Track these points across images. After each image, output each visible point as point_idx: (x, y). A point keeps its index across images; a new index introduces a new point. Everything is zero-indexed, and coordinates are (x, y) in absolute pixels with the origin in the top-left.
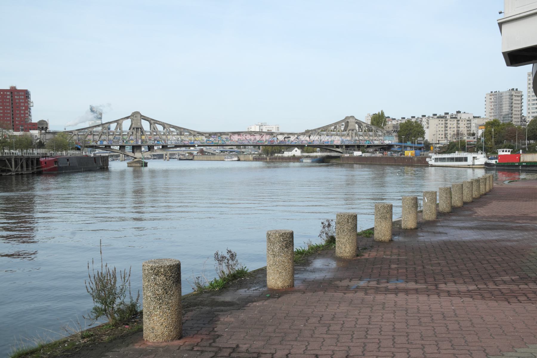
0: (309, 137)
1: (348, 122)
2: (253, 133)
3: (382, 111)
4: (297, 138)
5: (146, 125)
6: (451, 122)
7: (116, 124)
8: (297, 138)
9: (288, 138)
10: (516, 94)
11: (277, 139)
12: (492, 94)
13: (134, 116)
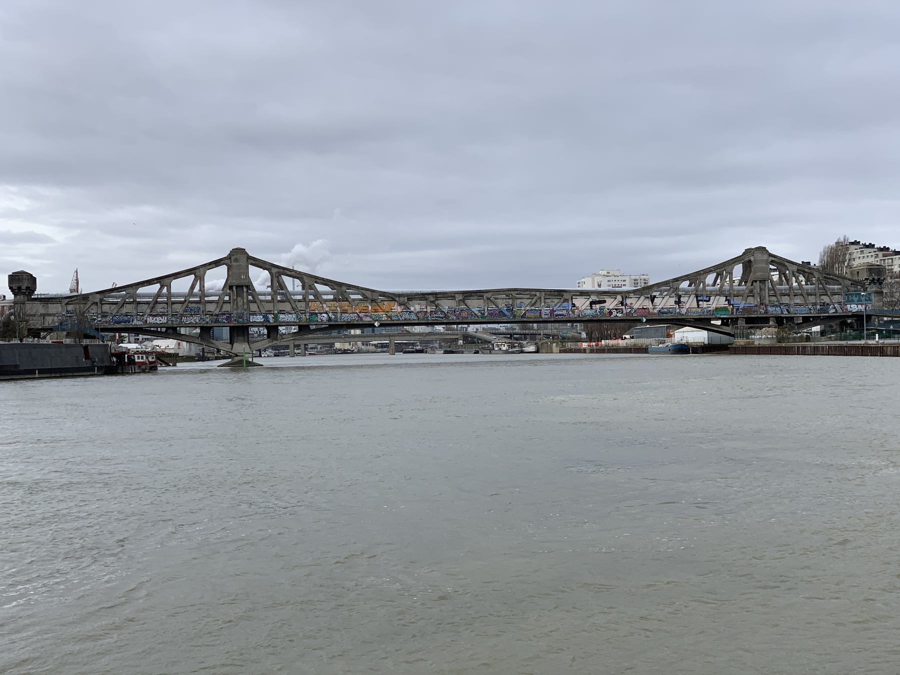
1: (750, 261)
2: (514, 293)
3: (845, 237)
4: (622, 303)
7: (193, 277)
8: (622, 303)
11: (574, 305)
13: (233, 258)
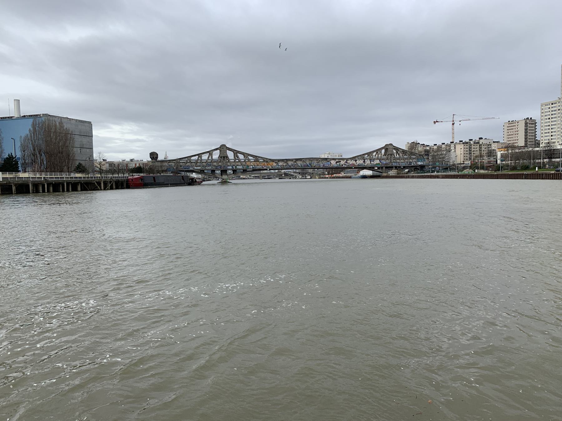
0: (356, 161)
4: (346, 162)
5: (230, 155)
6: (474, 147)
9: (339, 162)
10: (531, 122)
11: (331, 163)
12: (509, 123)
